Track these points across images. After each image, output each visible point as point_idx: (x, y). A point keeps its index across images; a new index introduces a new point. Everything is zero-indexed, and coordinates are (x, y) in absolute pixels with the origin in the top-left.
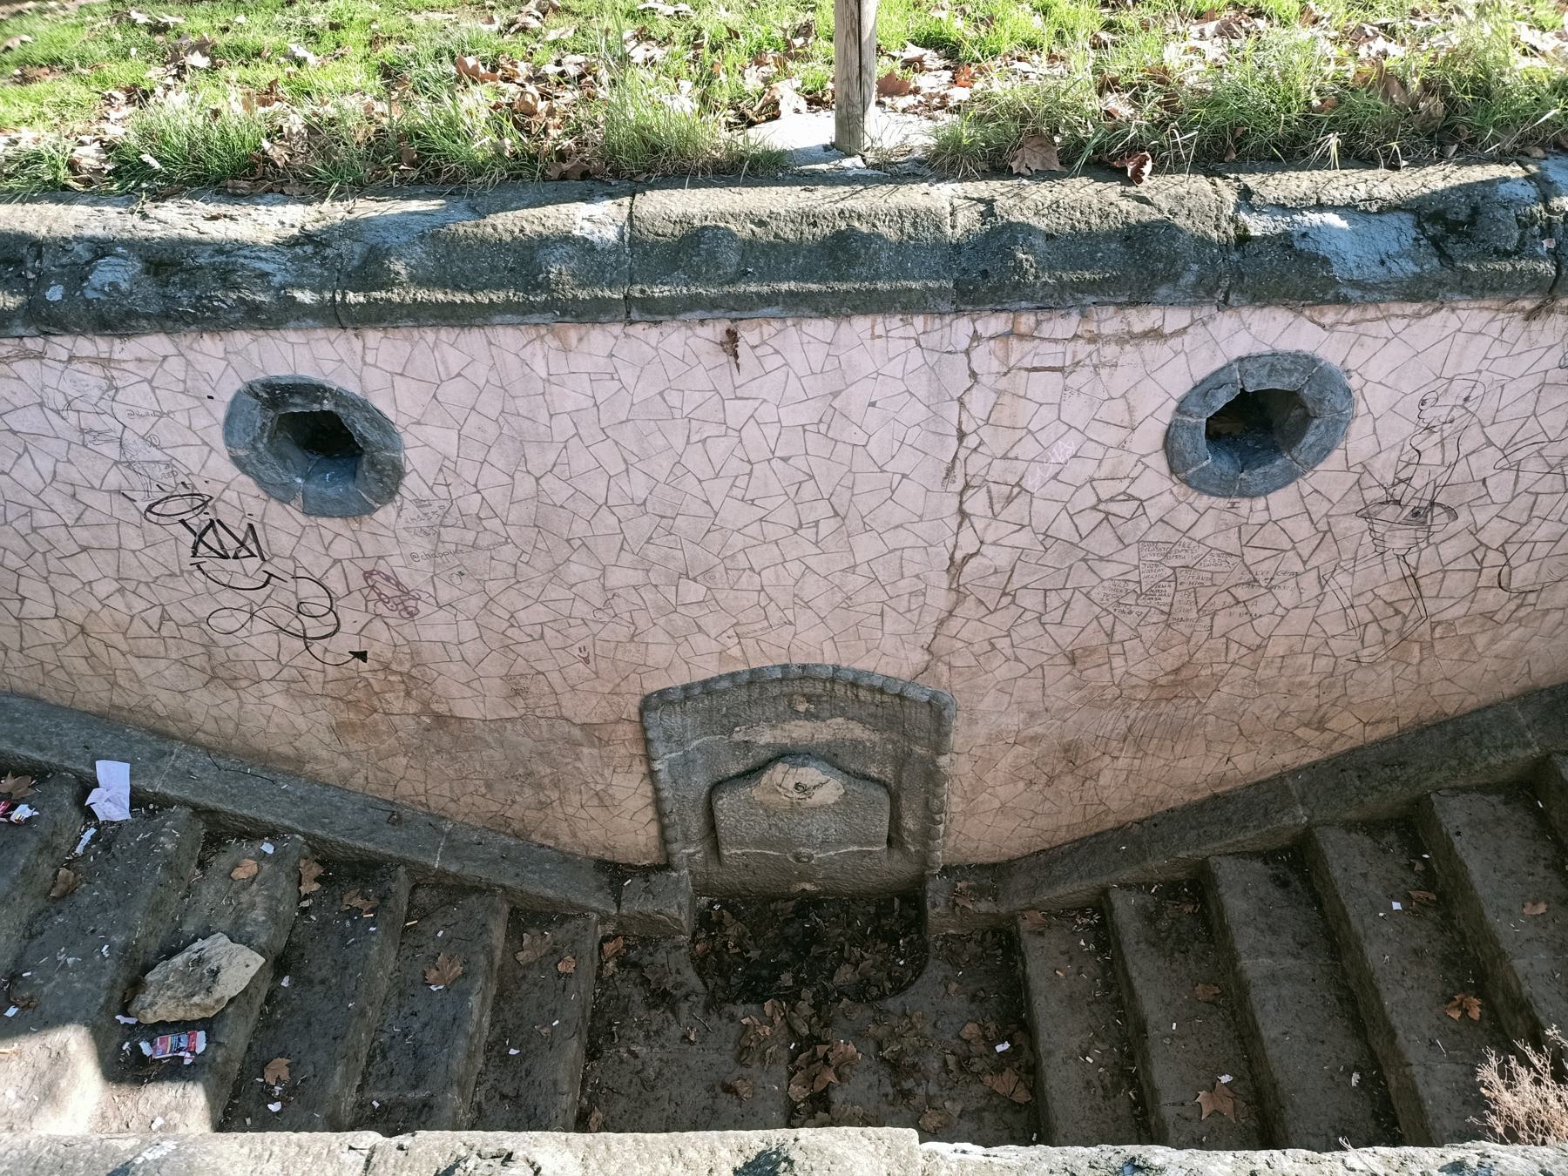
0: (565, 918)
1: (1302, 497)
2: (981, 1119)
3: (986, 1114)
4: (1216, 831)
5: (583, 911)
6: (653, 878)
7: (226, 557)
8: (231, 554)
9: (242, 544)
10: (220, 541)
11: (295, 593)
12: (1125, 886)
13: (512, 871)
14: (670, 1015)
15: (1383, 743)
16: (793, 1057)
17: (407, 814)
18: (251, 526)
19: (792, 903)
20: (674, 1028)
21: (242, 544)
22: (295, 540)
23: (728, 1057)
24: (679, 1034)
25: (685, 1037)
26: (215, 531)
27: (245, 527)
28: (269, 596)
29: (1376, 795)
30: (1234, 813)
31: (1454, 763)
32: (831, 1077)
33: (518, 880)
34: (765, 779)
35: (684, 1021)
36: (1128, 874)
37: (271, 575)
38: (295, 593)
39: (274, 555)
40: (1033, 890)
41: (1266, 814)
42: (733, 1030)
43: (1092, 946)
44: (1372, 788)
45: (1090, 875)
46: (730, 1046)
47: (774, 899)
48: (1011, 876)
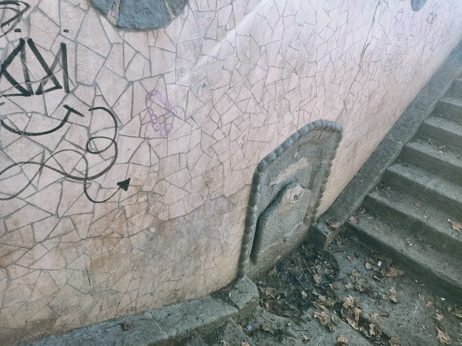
0: (222, 330)
1: (49, 251)
2: (401, 288)
3: (400, 285)
4: (383, 160)
5: (225, 321)
6: (237, 286)
7: (27, 93)
8: (35, 88)
9: (50, 72)
10: (26, 71)
11: (88, 128)
12: (370, 192)
13: (193, 318)
14: (289, 338)
15: (401, 117)
16: (340, 316)
17: (128, 321)
18: (63, 46)
19: (275, 269)
20: (296, 341)
21: (50, 72)
22: (101, 61)
23: (324, 334)
24: (301, 342)
25: (304, 340)
26: (23, 57)
27: (56, 48)
28: (63, 138)
29: (414, 128)
30: (383, 153)
31: (423, 112)
32: (358, 311)
33: (200, 321)
34: (284, 200)
35: (296, 335)
36: (370, 187)
37: (71, 110)
38: (88, 128)
39: (79, 83)
40: (347, 210)
41: (392, 148)
42: (314, 323)
43: (372, 217)
44: (411, 127)
45: (360, 194)
46: (320, 330)
47: (268, 272)
48: (334, 212)
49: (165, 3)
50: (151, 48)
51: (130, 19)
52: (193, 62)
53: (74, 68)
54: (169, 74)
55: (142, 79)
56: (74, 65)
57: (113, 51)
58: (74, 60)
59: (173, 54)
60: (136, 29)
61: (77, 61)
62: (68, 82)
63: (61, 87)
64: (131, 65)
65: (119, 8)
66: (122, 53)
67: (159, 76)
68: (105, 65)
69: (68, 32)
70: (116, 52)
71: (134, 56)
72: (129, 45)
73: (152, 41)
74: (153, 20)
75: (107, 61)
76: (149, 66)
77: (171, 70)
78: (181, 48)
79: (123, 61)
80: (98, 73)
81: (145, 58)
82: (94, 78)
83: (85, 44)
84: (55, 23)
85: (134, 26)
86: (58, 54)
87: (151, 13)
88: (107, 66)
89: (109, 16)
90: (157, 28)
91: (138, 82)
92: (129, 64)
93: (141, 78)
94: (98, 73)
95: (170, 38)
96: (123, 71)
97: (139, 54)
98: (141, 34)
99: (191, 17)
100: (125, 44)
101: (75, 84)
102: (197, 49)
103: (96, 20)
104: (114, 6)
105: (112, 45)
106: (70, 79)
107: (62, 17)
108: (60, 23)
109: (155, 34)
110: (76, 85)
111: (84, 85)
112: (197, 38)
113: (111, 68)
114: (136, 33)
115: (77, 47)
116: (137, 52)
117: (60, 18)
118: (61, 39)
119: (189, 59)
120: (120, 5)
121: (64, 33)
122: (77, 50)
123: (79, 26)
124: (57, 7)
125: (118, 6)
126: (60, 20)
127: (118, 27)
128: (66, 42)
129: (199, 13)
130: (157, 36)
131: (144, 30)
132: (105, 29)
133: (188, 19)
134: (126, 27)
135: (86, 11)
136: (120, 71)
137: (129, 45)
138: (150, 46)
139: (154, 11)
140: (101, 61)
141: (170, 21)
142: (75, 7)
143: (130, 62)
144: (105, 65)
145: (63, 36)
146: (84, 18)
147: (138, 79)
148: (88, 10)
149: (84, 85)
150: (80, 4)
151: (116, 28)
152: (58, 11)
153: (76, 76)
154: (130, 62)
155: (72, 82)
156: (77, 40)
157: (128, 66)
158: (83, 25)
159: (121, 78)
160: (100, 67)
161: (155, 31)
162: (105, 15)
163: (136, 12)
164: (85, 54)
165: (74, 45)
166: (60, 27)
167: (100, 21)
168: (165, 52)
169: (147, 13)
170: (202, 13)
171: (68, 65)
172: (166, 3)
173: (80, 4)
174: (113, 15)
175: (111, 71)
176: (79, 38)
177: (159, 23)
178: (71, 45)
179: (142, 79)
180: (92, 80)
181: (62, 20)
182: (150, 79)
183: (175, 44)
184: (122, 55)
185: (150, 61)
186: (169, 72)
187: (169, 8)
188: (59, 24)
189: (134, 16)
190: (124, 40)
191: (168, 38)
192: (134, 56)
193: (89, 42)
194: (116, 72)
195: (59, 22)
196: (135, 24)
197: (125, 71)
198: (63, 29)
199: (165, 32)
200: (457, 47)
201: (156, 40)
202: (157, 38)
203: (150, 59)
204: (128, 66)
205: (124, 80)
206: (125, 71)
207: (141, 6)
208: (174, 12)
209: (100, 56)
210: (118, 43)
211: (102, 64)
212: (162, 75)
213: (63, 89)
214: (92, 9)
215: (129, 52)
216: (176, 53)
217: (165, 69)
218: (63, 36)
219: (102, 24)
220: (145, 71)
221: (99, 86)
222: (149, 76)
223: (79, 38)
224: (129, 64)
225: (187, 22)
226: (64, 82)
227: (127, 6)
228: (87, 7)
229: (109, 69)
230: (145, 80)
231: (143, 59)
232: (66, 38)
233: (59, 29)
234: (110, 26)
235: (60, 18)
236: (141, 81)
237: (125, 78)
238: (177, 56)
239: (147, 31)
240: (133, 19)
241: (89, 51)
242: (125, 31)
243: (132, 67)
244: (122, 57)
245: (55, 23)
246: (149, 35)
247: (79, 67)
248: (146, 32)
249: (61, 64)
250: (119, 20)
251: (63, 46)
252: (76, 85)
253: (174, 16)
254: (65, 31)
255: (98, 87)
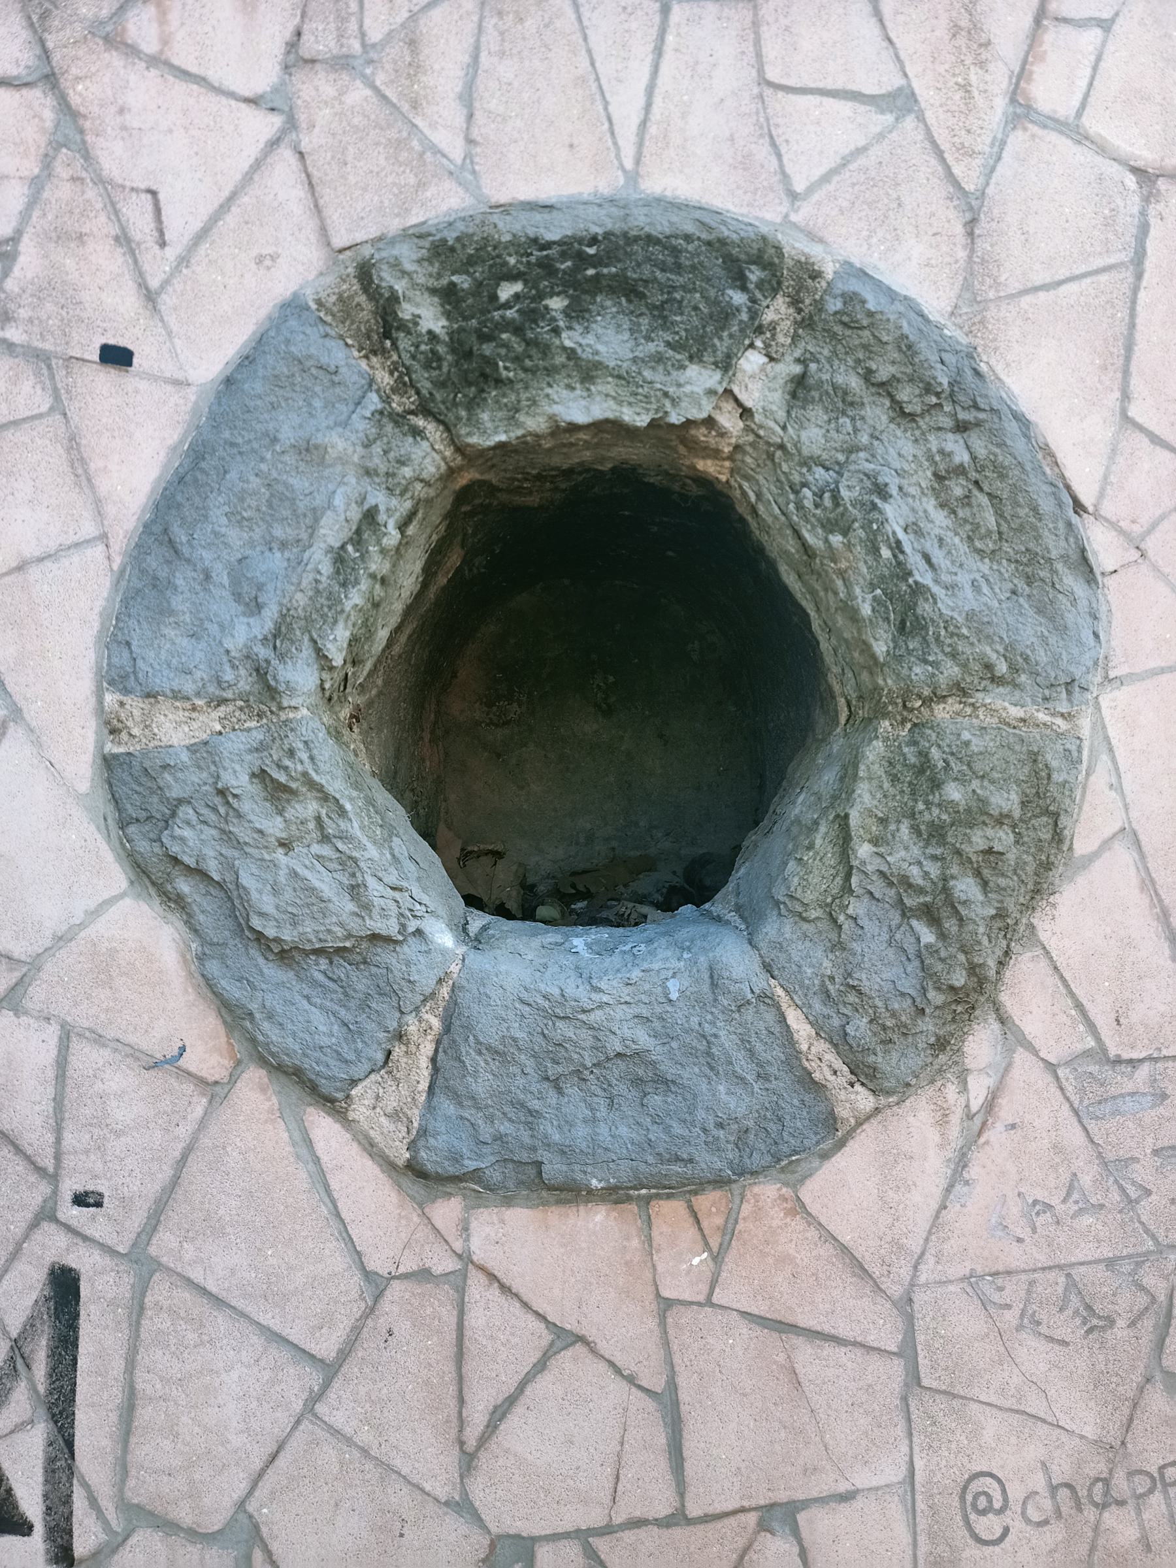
18: (64, 1287)
22: (297, 1382)
49: (782, 1019)
50: (679, 1318)
51: (505, 1127)
52: (1090, 1432)
53: (114, 1417)
54: (844, 1508)
55: (608, 1530)
56: (115, 1395)
57: (383, 1323)
58: (118, 1365)
59: (876, 1364)
60: (543, 1183)
61: (141, 1377)
62: (67, 1500)
63: (23, 1528)
64: (513, 1421)
65: (433, 1060)
66: (451, 1336)
67: (752, 1519)
68: (320, 1408)
69: (99, 1205)
70: (403, 1328)
71: (541, 1366)
72: (505, 1289)
73: (684, 1266)
74: (678, 1129)
75: (337, 1384)
76: (662, 1440)
77: (862, 1479)
78: (955, 1323)
79: (452, 1389)
80: (274, 1457)
81: (631, 1380)
82: (242, 1487)
83: (196, 1275)
84: (28, 1158)
85: (532, 1171)
86: (30, 1326)
87: (664, 1083)
88: (338, 1419)
89: (360, 1111)
90: (720, 1182)
91: (572, 1550)
92: (500, 1413)
93: (596, 1518)
94: (274, 1457)
95: (844, 1249)
96: (452, 1458)
97: (579, 1348)
98: (598, 1219)
99: (1032, 1099)
100: (476, 1286)
101: (111, 1514)
102: (1120, 1330)
103: (279, 1136)
104: (398, 1051)
105: (376, 1285)
106: (85, 1485)
107: (69, 1125)
108: (58, 1157)
109: (713, 1221)
110: (116, 1524)
111: (167, 1526)
112: (1107, 1253)
113: (365, 1436)
114: (554, 1214)
115: (143, 1294)
116: (564, 1338)
117: (58, 1131)
118: (53, 1247)
119: (1035, 1405)
120: (438, 1042)
121: (76, 1211)
122: (142, 1308)
123: (168, 1172)
124: (51, 1074)
125: (428, 1048)
126: (58, 1140)
127: (419, 1176)
128: (83, 1261)
129: (1108, 1072)
130: (729, 1231)
131: (615, 1195)
132: (334, 1185)
133: (1007, 1111)
134: (475, 1175)
135: (215, 1091)
136: (434, 1467)
137: (505, 1289)
138: (666, 1305)
139: (690, 1074)
140: (297, 1382)
141: (832, 1132)
142: (156, 1065)
143: (511, 1401)
144: (320, 1408)
145: (68, 1228)
146: (202, 1124)
147: (569, 1528)
148: (233, 1079)
149: (167, 1526)
150: (183, 1049)
151: (407, 1182)
152: (51, 1091)
153: (123, 1468)
154: (511, 1401)
155: (93, 1502)
156: (153, 1250)
157: (492, 1427)
158: (194, 1165)
159: (431, 1507)
160: (284, 1420)
161: (709, 1202)
162: (334, 1104)
163: (557, 1084)
164: (192, 1337)
165: (128, 1280)
166: (54, 1178)
167: (309, 1143)
168: (805, 1354)
169: (637, 1082)
170: (1144, 1071)
171: (79, 1398)
172: (794, 1018)
173: (183, 1049)
174: (391, 1103)
175: (365, 1452)
176: (164, 1244)
177: (740, 1142)
178: (110, 1278)
179: (608, 1530)
180: (227, 1503)
181: (69, 1139)
182: (677, 1532)
183: (896, 1291)
184: (451, 1351)
185: (676, 1403)
186: (846, 1497)
187: (821, 1046)
188: (49, 1164)
189: (535, 1104)
190: (465, 1258)
191: (826, 1251)
192: (541, 1366)
193: (221, 1265)
194: (398, 1462)
195: (50, 1151)
196: (543, 1155)
197: (468, 1461)
198: (70, 1185)
199: (799, 1208)
200: (791, 760)
201: (717, 1258)
202: (724, 1248)
203: (672, 1385)
204: (492, 1427)
205: (453, 1528)
206: (468, 1461)
207: (590, 1042)
208: (863, 1072)
209: (285, 1354)
210: (423, 1275)
211: (298, 1406)
212: (780, 1516)
213: (37, 1542)
214: (254, 1075)
215: (503, 1338)
216: (908, 1351)
217: (809, 1471)
218: (68, 1228)
219: (317, 1160)
220: (627, 1475)
221: (274, 1546)
222: (662, 1508)
223: (164, 1244)
224: (500, 1413)
225: (996, 1134)
226: (46, 1497)
227: (482, 1048)
228: (228, 1063)
229: (349, 1441)
230: (628, 1536)
231: (617, 1388)
232: (85, 1238)
233: (45, 1188)
234: (370, 1169)
235: (58, 1131)
236: (601, 1545)
237: (463, 1506)
238: (913, 1378)
239: (648, 1200)
240: (530, 1126)
241: (222, 1322)
242: (476, 1202)
243: (517, 1433)
244: (449, 1368)
245: (28, 1158)
246: (660, 1230)
247: (145, 1414)
248: (634, 1207)
249: (42, 1389)
250: (423, 1132)
251: (64, 1287)
252: (116, 1524)
253: (864, 1100)
254: (80, 1200)
255: (269, 1553)
